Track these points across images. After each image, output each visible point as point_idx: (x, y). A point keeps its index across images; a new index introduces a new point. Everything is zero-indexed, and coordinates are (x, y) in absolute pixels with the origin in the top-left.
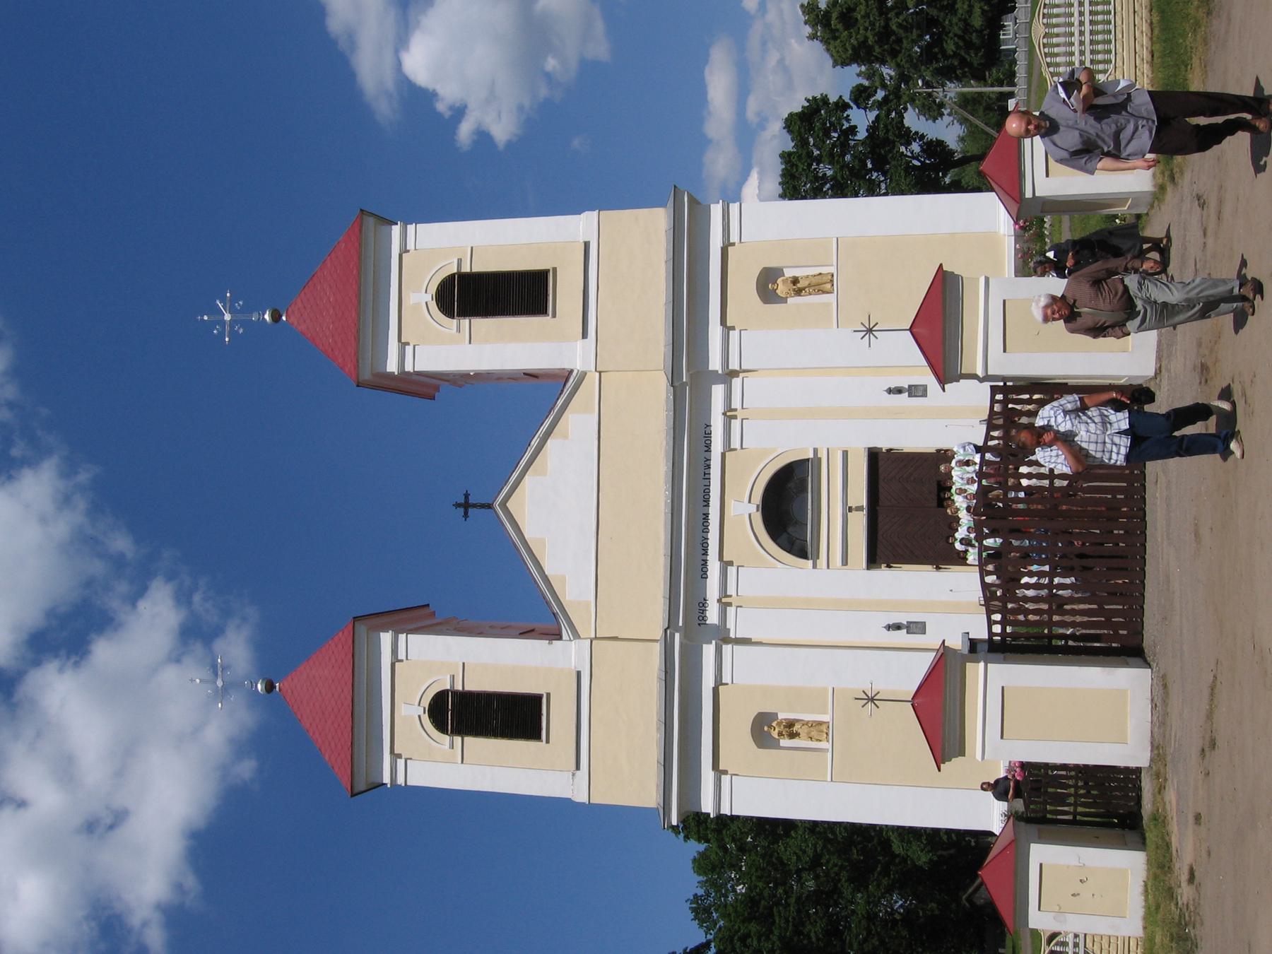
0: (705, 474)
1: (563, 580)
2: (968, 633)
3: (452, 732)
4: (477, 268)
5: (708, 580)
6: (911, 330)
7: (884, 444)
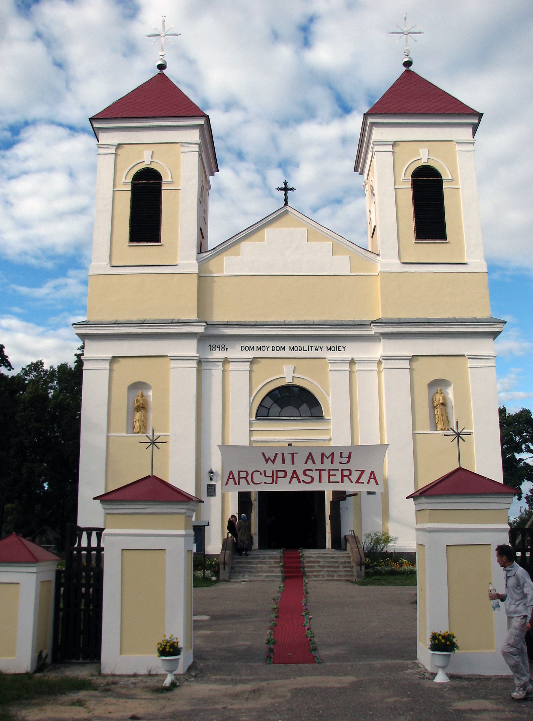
1: (237, 254)
2: (208, 525)
3: (133, 183)
4: (446, 193)
5: (355, 320)
6: (460, 469)
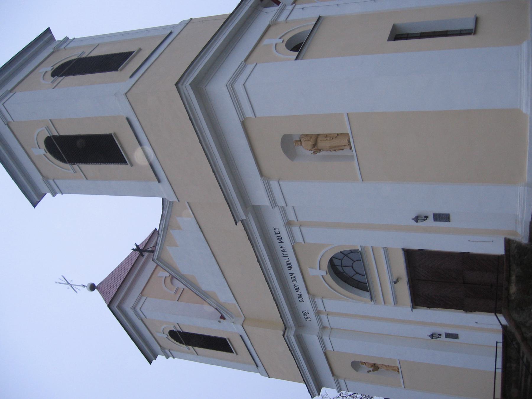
0: (283, 254)
7: (415, 246)
